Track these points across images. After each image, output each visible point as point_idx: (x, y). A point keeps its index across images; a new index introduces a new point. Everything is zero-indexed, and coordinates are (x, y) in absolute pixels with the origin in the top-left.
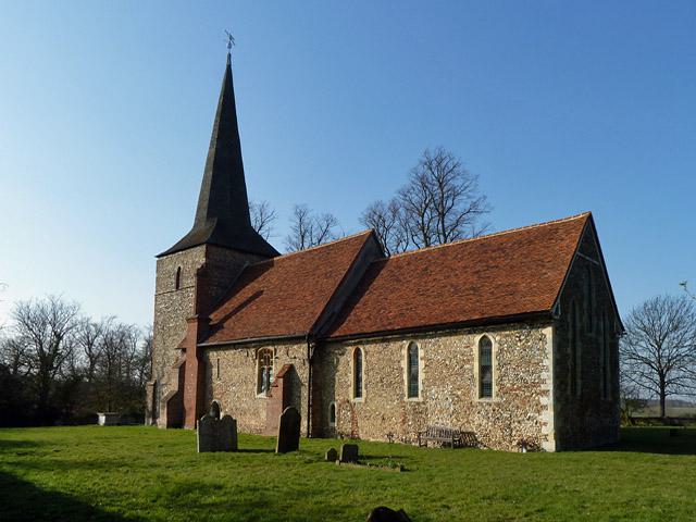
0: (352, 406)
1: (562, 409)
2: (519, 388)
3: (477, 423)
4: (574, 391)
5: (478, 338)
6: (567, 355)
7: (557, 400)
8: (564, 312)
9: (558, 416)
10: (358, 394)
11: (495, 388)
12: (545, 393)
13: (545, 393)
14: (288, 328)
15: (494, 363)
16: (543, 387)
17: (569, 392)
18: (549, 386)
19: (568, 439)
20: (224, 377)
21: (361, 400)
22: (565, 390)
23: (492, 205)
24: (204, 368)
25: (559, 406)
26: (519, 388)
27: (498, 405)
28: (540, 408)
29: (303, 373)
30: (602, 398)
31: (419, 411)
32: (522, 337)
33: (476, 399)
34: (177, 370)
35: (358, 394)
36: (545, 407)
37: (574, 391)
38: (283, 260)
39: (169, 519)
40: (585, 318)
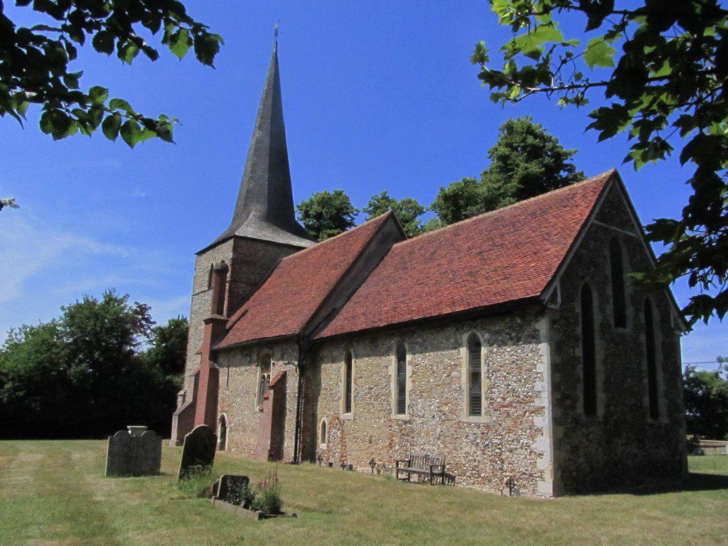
0: (342, 423)
1: (565, 434)
2: (510, 405)
3: (464, 453)
4: (590, 407)
5: (465, 337)
6: (575, 358)
7: (557, 421)
8: (568, 298)
9: (558, 444)
10: (348, 409)
11: (484, 403)
12: (539, 411)
13: (539, 411)
14: (284, 327)
15: (484, 369)
16: (537, 403)
17: (580, 409)
18: (545, 401)
19: (576, 477)
20: (232, 386)
21: (350, 415)
22: (573, 407)
23: (578, 171)
24: (214, 375)
25: (561, 430)
26: (510, 405)
27: (488, 427)
28: (535, 432)
29: (292, 384)
30: (649, 420)
31: (406, 432)
32: (514, 334)
33: (464, 416)
34: (193, 378)
35: (348, 409)
36: (539, 430)
37: (590, 407)
38: (310, 252)
39: (361, 544)
40: (610, 308)
